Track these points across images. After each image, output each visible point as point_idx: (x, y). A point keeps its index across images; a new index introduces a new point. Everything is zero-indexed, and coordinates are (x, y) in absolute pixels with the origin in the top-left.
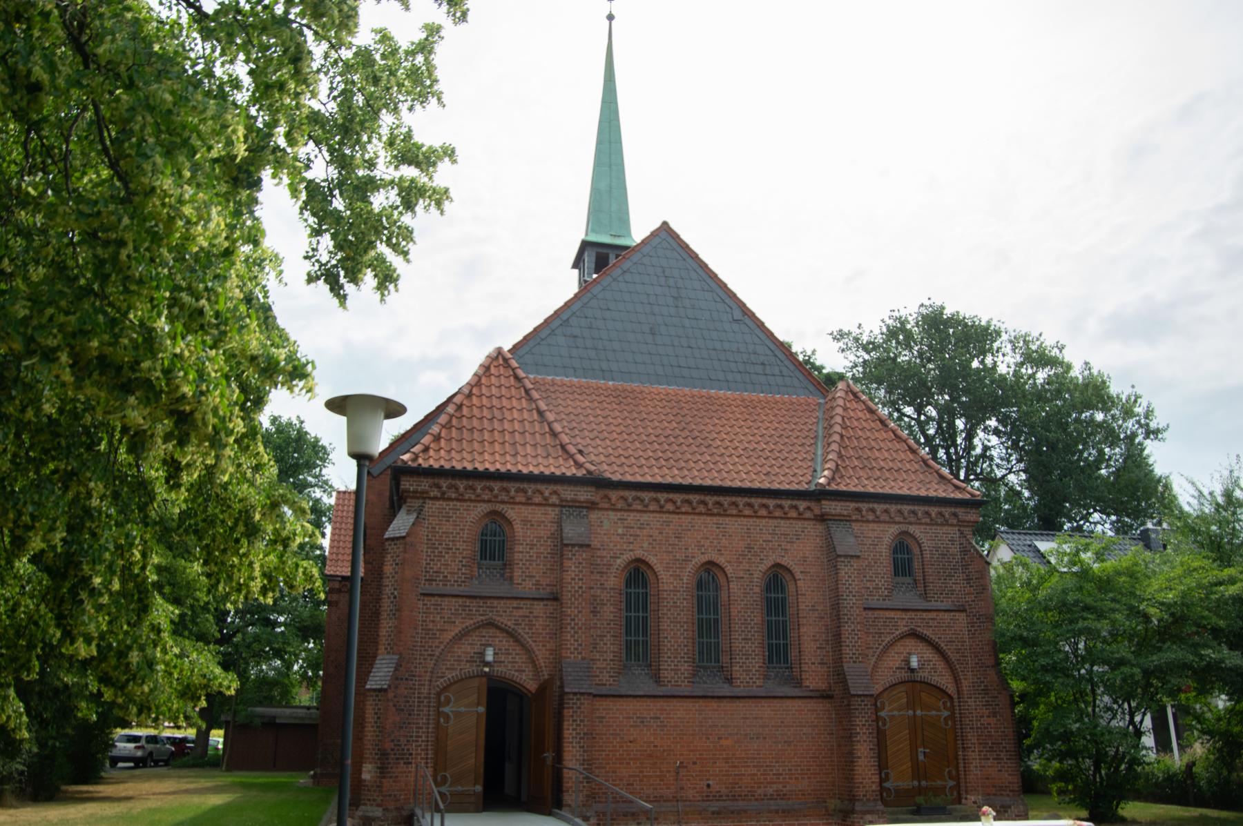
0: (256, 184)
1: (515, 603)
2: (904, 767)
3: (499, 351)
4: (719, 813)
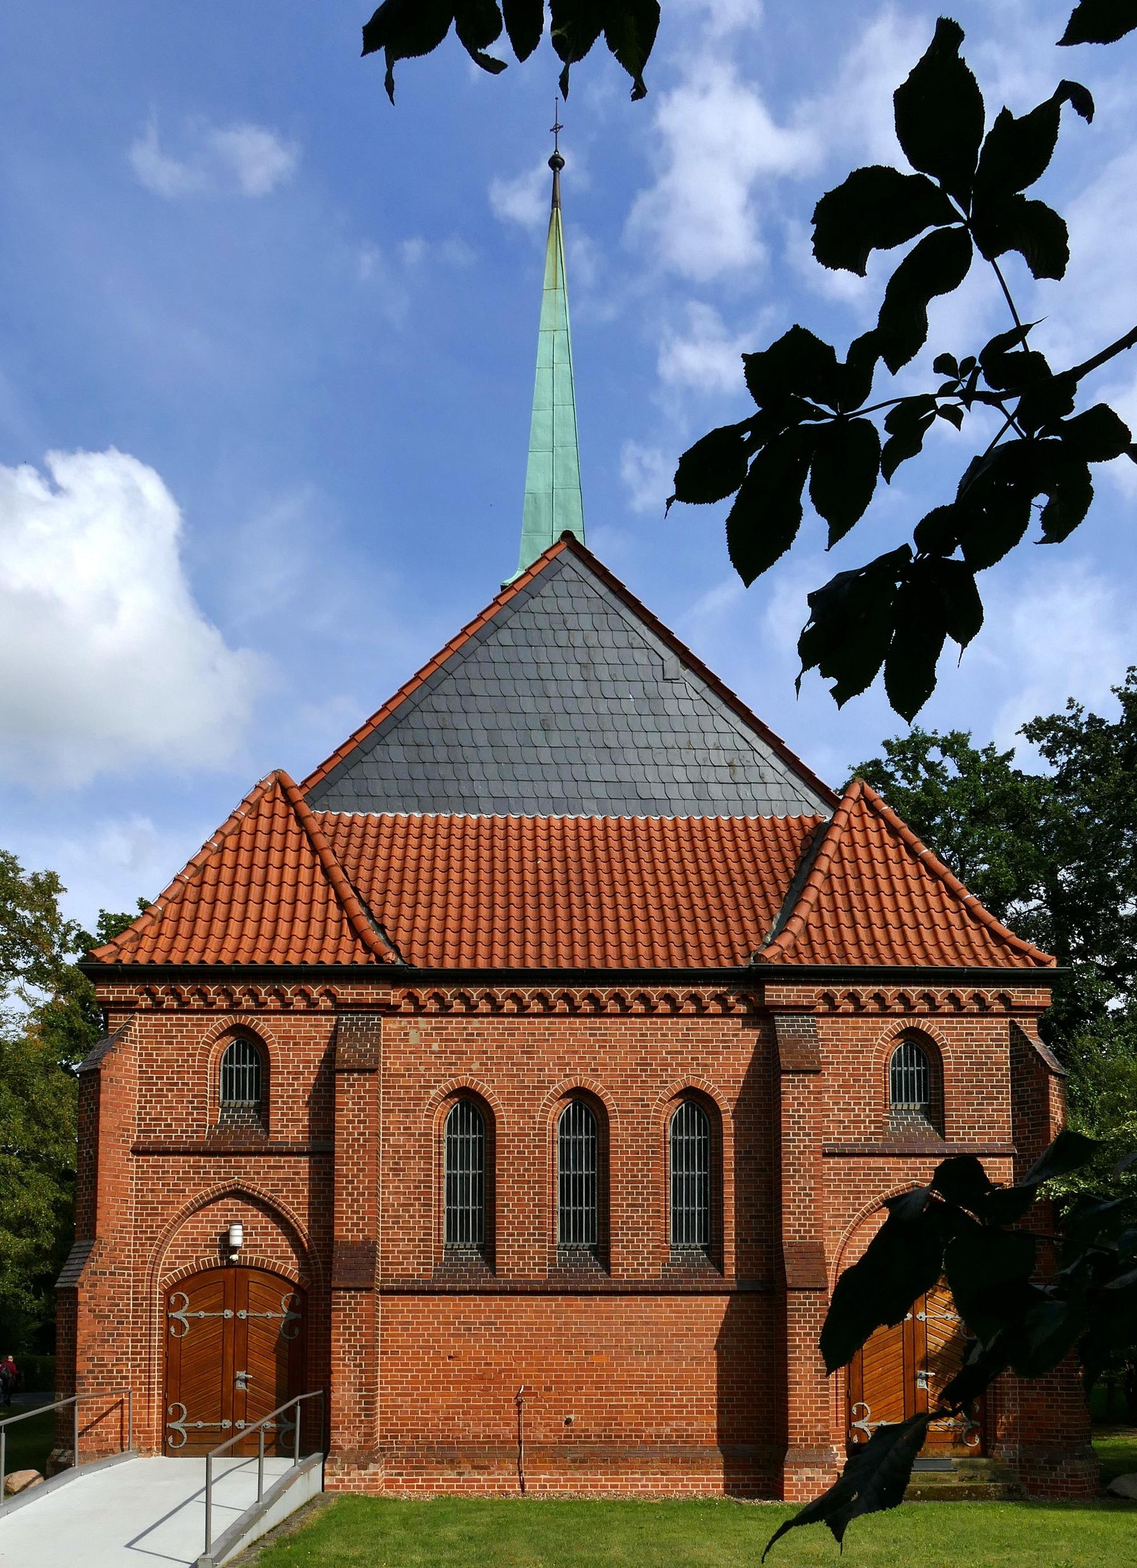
0: (1018, 773)
1: (272, 1160)
2: (893, 1398)
3: (280, 781)
4: (583, 1461)
